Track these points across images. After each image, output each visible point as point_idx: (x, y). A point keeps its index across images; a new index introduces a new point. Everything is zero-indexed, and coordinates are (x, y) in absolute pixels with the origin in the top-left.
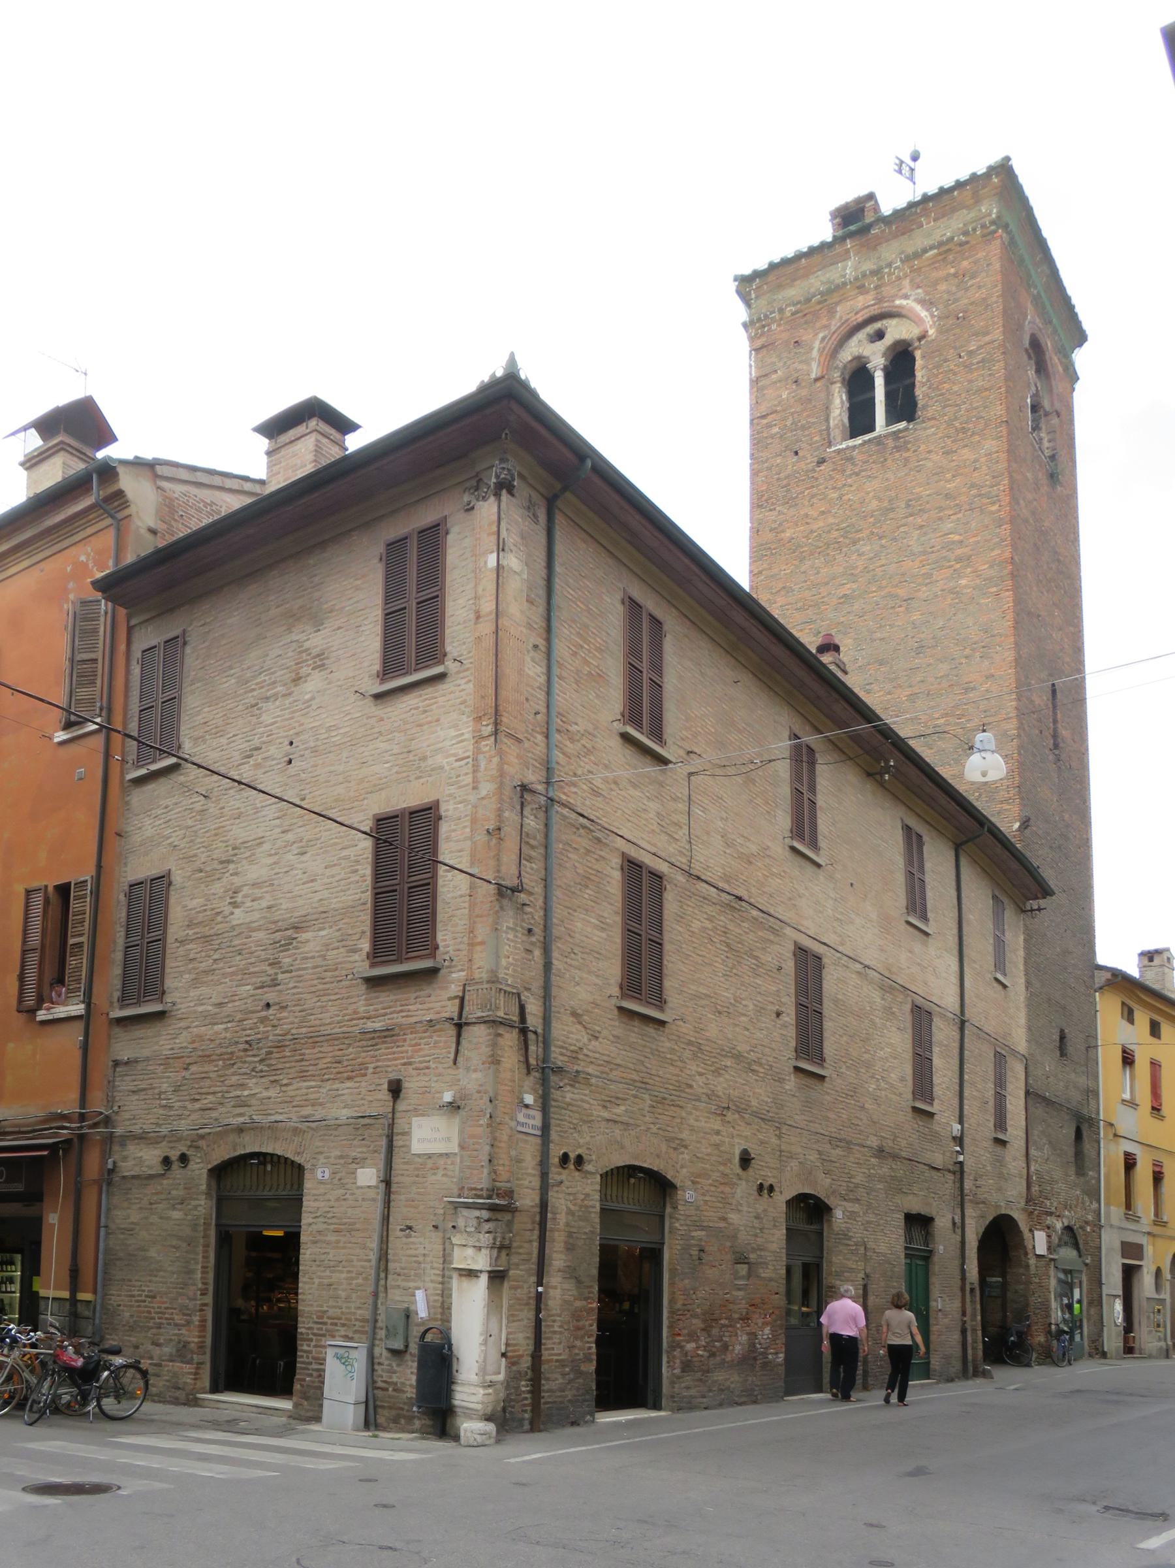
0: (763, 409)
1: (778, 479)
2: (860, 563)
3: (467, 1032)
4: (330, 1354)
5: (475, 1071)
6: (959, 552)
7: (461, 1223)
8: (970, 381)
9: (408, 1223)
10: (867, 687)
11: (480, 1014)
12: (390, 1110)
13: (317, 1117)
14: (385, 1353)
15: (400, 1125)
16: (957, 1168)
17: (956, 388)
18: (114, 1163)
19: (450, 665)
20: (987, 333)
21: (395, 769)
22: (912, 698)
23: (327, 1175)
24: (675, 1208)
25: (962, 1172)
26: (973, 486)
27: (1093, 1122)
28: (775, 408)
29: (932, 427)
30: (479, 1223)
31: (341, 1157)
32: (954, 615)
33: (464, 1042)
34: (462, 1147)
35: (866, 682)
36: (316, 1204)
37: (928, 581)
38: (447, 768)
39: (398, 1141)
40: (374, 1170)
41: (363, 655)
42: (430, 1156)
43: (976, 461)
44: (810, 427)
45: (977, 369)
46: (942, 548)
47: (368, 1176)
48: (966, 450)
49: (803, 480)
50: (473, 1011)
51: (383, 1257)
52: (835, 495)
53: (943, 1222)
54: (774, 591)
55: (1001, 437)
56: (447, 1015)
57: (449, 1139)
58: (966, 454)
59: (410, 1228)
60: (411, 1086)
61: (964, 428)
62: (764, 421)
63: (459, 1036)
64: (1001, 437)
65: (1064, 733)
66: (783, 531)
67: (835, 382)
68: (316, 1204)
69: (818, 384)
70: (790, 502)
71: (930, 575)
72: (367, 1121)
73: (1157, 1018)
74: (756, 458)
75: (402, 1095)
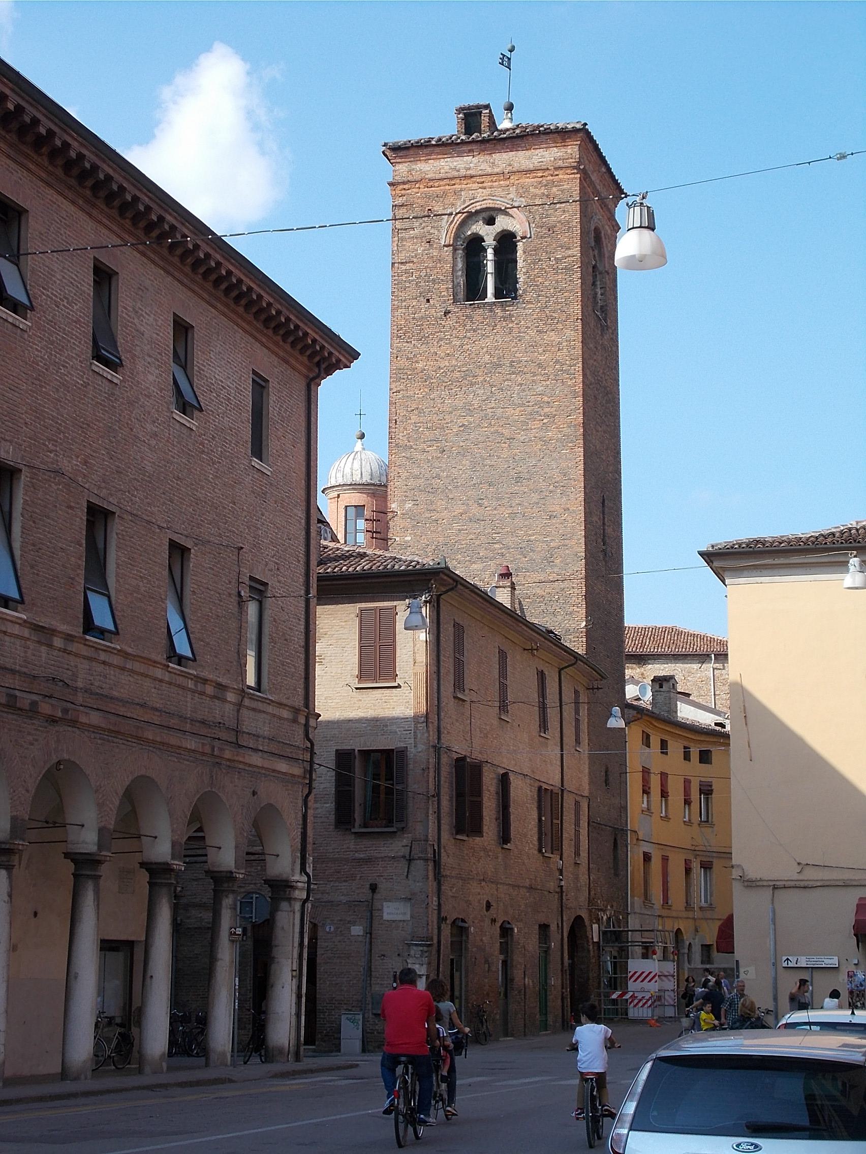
0: (402, 256)
1: (414, 318)
2: (476, 403)
3: (414, 863)
4: (343, 1017)
5: (418, 882)
6: (546, 410)
7: (412, 953)
8: (557, 282)
9: (382, 953)
10: (480, 501)
11: (420, 855)
12: (370, 898)
13: (325, 900)
14: (371, 1015)
15: (377, 904)
16: (558, 890)
17: (547, 283)
18: (181, 920)
19: (399, 681)
20: (569, 249)
21: (369, 728)
22: (513, 515)
23: (332, 929)
24: (468, 937)
25: (562, 892)
26: (557, 362)
27: (624, 831)
28: (412, 259)
29: (530, 308)
30: (422, 953)
31: (341, 920)
32: (543, 458)
33: (412, 868)
34: (412, 917)
35: (479, 497)
36: (326, 944)
37: (524, 427)
38: (399, 733)
39: (376, 913)
40: (361, 928)
41: (347, 663)
42: (394, 921)
43: (560, 343)
44: (439, 283)
45: (562, 273)
46: (536, 404)
47: (357, 930)
48: (552, 333)
49: (433, 325)
50: (416, 853)
51: (369, 970)
52: (458, 343)
53: (553, 927)
54: (409, 409)
55: (577, 330)
56: (402, 854)
57: (405, 914)
58: (553, 336)
59: (384, 956)
60: (383, 886)
61: (551, 316)
62: (404, 267)
63: (409, 864)
64: (577, 330)
65: (609, 530)
66: (417, 362)
67: (459, 249)
68: (326, 944)
69: (446, 249)
70: (423, 339)
71: (525, 423)
72: (356, 903)
73: (665, 737)
74: (396, 296)
75: (377, 891)
